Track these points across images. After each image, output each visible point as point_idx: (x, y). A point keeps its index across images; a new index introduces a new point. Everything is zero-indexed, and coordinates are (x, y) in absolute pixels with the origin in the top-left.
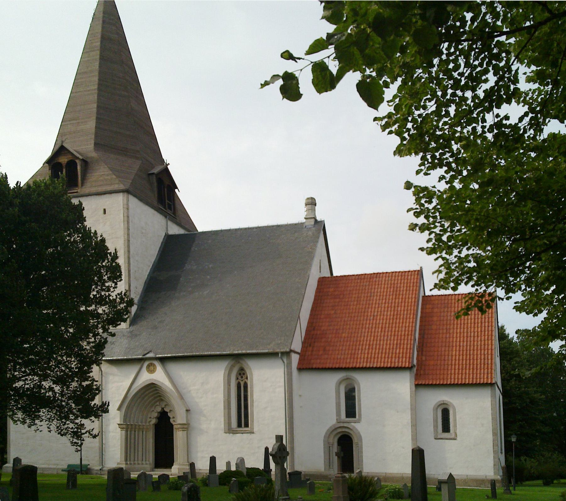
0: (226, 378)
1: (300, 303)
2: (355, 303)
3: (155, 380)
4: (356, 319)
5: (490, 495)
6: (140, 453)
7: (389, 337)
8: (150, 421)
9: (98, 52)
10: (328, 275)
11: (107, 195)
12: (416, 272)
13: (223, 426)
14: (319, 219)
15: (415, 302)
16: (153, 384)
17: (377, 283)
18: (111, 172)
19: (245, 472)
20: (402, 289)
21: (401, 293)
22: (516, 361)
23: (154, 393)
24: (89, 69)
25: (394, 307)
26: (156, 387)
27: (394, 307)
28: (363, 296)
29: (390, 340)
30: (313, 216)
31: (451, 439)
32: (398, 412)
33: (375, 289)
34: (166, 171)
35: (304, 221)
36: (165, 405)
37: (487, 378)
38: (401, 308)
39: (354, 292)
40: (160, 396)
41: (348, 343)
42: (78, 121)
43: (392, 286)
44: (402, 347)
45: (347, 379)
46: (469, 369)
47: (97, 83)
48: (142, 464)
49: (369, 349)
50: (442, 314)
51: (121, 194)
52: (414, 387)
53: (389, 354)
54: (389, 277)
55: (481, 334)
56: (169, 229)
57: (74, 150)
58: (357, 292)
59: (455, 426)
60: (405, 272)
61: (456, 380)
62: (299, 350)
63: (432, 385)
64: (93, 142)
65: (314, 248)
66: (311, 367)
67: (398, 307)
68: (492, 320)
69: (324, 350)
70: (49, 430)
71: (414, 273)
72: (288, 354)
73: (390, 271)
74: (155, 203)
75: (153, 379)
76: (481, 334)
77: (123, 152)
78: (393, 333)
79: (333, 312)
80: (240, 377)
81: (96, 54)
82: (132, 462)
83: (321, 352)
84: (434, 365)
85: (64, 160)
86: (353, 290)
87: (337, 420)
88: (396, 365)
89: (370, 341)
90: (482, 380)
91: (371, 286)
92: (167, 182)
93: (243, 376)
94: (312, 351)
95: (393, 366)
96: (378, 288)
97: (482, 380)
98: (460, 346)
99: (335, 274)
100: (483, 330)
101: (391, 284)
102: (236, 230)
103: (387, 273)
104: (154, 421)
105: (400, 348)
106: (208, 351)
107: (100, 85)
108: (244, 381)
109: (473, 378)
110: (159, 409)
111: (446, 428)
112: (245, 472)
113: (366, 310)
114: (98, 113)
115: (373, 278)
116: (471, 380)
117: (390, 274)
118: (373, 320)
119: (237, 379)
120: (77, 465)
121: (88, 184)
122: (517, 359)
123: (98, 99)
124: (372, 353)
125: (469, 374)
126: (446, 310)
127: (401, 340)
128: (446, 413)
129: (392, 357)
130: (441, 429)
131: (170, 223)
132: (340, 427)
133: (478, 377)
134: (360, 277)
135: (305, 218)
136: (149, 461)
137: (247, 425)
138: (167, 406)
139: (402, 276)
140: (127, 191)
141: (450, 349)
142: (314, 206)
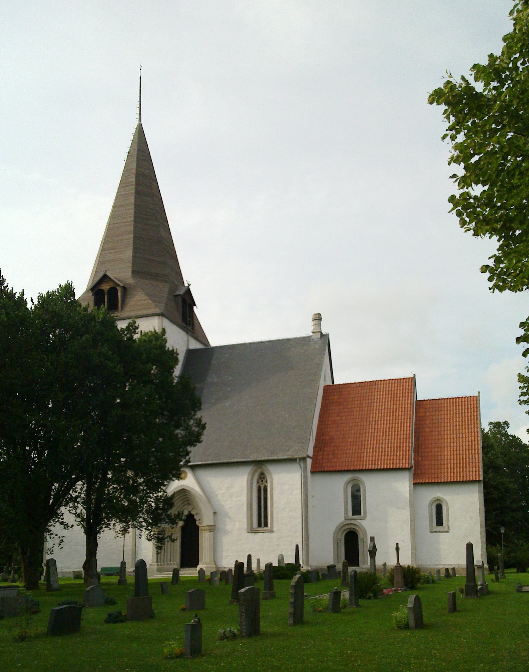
1: (313, 412)
3: (188, 487)
4: (359, 424)
5: (495, 580)
6: (169, 555)
7: (390, 440)
9: (134, 187)
10: (331, 384)
11: (145, 318)
12: (410, 380)
13: (246, 526)
14: (324, 332)
15: (410, 407)
16: (184, 489)
17: (376, 390)
18: (147, 298)
19: (284, 566)
20: (398, 395)
21: (398, 399)
22: (492, 454)
23: (184, 497)
24: (126, 202)
25: (393, 412)
26: (186, 492)
27: (393, 412)
28: (364, 402)
29: (391, 443)
30: (319, 330)
31: (444, 532)
32: (398, 509)
33: (375, 396)
34: (188, 291)
35: (312, 334)
36: (193, 509)
37: (476, 475)
38: (399, 413)
39: (356, 399)
40: (188, 500)
41: (354, 447)
42: (116, 250)
43: (390, 392)
44: (401, 449)
45: (354, 480)
46: (460, 468)
47: (133, 215)
48: (171, 564)
49: (373, 452)
50: (434, 418)
51: (157, 317)
52: (413, 486)
53: (391, 456)
54: (386, 384)
55: (468, 435)
56: (190, 344)
57: (114, 277)
58: (359, 399)
59: (448, 519)
60: (400, 379)
61: (449, 478)
62: (311, 455)
63: (428, 483)
64: (130, 270)
65: (322, 359)
66: (323, 470)
67: (396, 412)
68: (477, 421)
69: (334, 454)
70: (140, 536)
71: (409, 380)
72: (304, 459)
73: (387, 379)
74: (180, 320)
76: (468, 435)
77: (155, 277)
78: (393, 437)
79: (338, 418)
81: (132, 189)
82: (169, 563)
83: (330, 456)
84: (429, 465)
85: (106, 287)
86: (355, 397)
87: (345, 517)
88: (398, 467)
89: (373, 444)
90: (471, 477)
91: (370, 393)
92: (188, 301)
94: (323, 455)
95: (395, 467)
96: (377, 395)
97: (471, 477)
98: (450, 447)
99: (336, 383)
100: (470, 431)
101: (389, 391)
102: (250, 344)
103: (384, 380)
105: (400, 451)
106: (234, 458)
107: (135, 217)
109: (463, 476)
111: (440, 522)
112: (284, 566)
113: (368, 416)
114: (135, 243)
115: (373, 385)
116: (462, 477)
117: (388, 381)
118: (375, 424)
119: (258, 482)
120: (117, 568)
121: (127, 309)
122: (493, 452)
123: (134, 230)
124: (375, 456)
125: (460, 472)
126: (437, 413)
127: (400, 443)
128: (439, 508)
129: (393, 460)
130: (436, 523)
132: (348, 524)
133: (468, 475)
134: (361, 384)
135: (313, 332)
136: (176, 561)
137: (266, 525)
138: (194, 510)
139: (397, 383)
140: (162, 315)
141: (443, 450)
142: (320, 321)
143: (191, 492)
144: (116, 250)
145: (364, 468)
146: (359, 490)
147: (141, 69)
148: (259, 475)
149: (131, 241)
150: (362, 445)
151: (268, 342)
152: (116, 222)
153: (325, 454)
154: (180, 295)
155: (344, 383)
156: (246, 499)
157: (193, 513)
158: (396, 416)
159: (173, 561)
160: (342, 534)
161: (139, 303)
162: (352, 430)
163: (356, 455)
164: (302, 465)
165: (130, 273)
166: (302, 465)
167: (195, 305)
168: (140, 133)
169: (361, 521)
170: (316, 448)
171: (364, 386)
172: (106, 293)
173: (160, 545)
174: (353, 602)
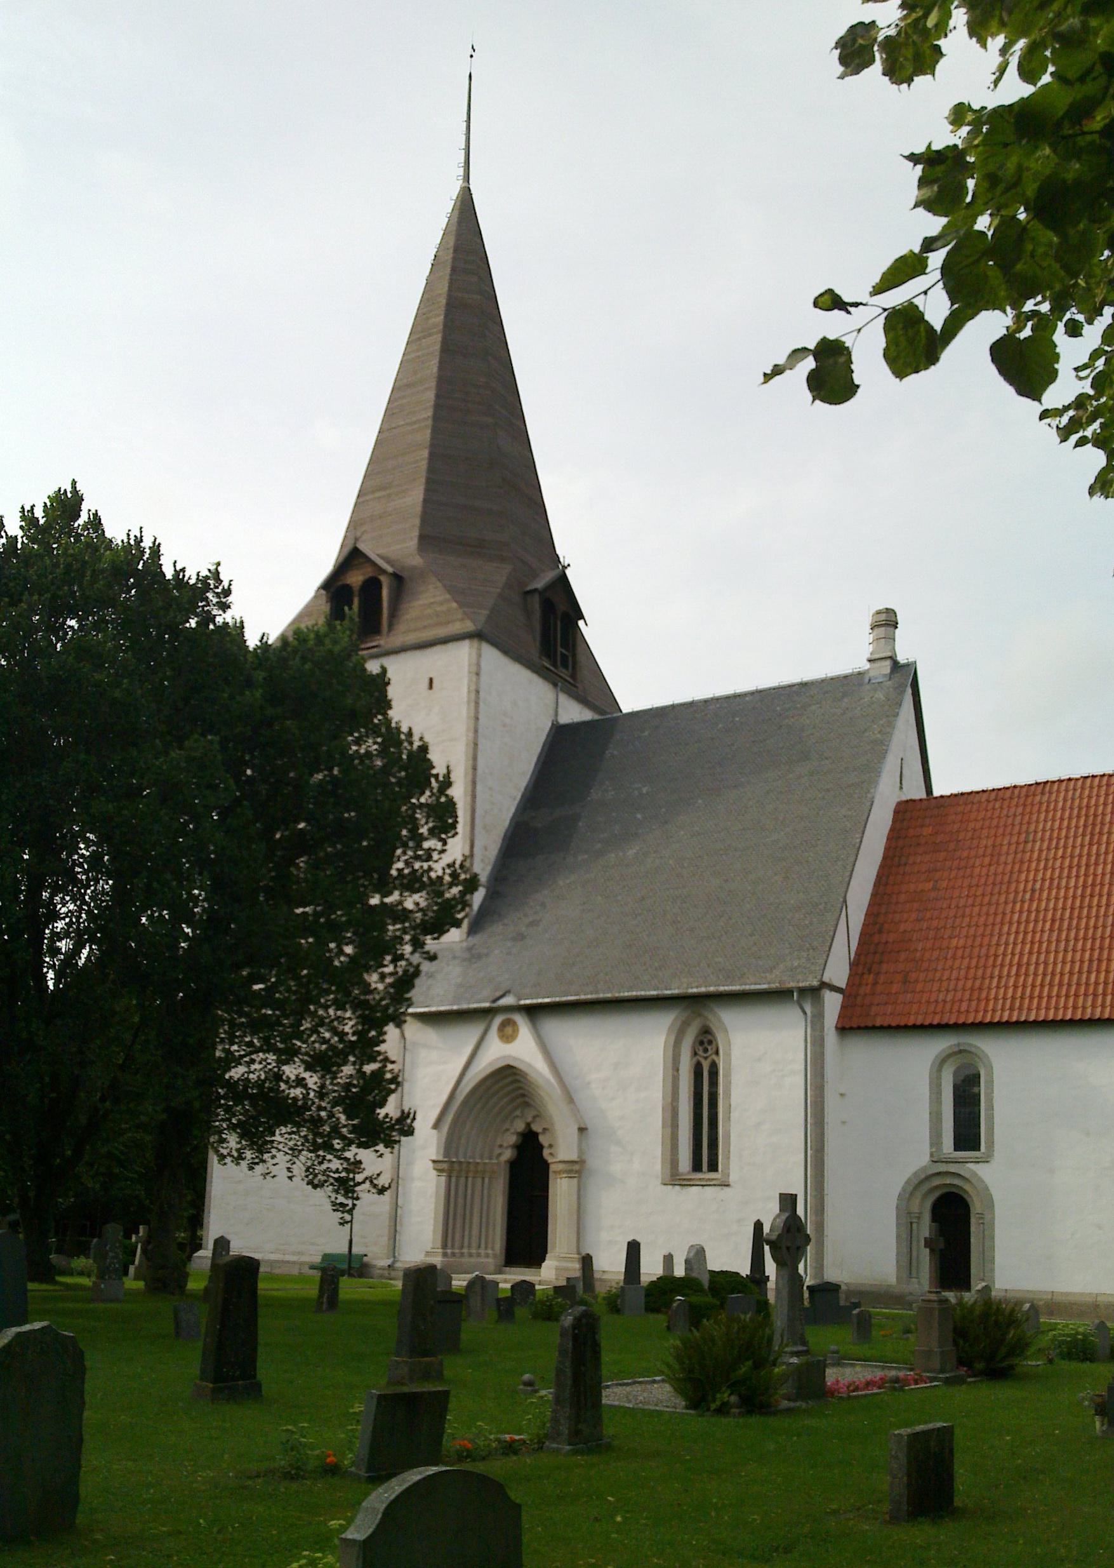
0: (670, 1053)
1: (849, 868)
2: (987, 860)
3: (515, 1059)
6: (475, 1232)
8: (500, 1155)
14: (902, 658)
17: (1044, 807)
23: (511, 1087)
26: (515, 1074)
30: (889, 654)
35: (867, 666)
36: (534, 1117)
51: (467, 643)
56: (560, 710)
65: (888, 729)
66: (870, 1024)
74: (533, 649)
75: (509, 1057)
80: (701, 1053)
81: (435, 342)
83: (895, 988)
85: (356, 579)
87: (932, 1155)
92: (562, 607)
93: (709, 1048)
94: (875, 983)
99: (936, 793)
101: (1080, 808)
104: (508, 1154)
106: (631, 989)
107: (437, 407)
108: (709, 1060)
110: (520, 1126)
114: (431, 470)
115: (1034, 795)
119: (695, 1054)
121: (401, 627)
124: (1024, 986)
131: (563, 698)
132: (939, 1174)
135: (870, 661)
137: (713, 1167)
138: (538, 1119)
140: (478, 636)
142: (891, 629)
143: (526, 1074)
144: (388, 492)
145: (988, 1020)
146: (974, 1080)
147: (472, 56)
148: (697, 1037)
149: (424, 465)
150: (987, 956)
151: (752, 693)
152: (393, 426)
153: (881, 981)
154: (536, 590)
155: (955, 791)
156: (660, 1095)
157: (536, 1128)
158: (1095, 875)
159: (486, 1248)
160: (925, 1196)
161: (429, 611)
162: (963, 916)
163: (969, 984)
164: (808, 1010)
165: (413, 543)
166: (808, 1010)
167: (582, 617)
168: (465, 210)
169: (977, 1166)
170: (857, 965)
171: (1011, 798)
172: (356, 593)
173: (341, 1199)
174: (564, 1429)
